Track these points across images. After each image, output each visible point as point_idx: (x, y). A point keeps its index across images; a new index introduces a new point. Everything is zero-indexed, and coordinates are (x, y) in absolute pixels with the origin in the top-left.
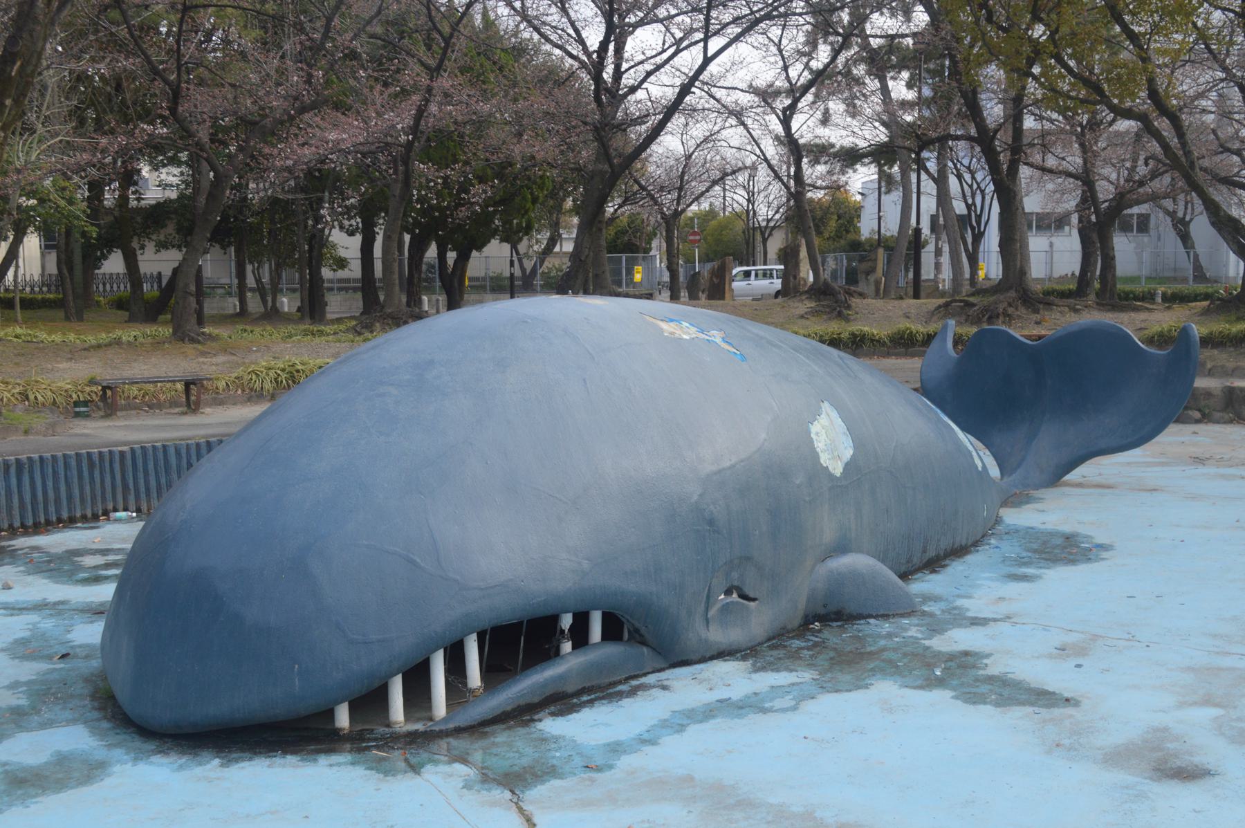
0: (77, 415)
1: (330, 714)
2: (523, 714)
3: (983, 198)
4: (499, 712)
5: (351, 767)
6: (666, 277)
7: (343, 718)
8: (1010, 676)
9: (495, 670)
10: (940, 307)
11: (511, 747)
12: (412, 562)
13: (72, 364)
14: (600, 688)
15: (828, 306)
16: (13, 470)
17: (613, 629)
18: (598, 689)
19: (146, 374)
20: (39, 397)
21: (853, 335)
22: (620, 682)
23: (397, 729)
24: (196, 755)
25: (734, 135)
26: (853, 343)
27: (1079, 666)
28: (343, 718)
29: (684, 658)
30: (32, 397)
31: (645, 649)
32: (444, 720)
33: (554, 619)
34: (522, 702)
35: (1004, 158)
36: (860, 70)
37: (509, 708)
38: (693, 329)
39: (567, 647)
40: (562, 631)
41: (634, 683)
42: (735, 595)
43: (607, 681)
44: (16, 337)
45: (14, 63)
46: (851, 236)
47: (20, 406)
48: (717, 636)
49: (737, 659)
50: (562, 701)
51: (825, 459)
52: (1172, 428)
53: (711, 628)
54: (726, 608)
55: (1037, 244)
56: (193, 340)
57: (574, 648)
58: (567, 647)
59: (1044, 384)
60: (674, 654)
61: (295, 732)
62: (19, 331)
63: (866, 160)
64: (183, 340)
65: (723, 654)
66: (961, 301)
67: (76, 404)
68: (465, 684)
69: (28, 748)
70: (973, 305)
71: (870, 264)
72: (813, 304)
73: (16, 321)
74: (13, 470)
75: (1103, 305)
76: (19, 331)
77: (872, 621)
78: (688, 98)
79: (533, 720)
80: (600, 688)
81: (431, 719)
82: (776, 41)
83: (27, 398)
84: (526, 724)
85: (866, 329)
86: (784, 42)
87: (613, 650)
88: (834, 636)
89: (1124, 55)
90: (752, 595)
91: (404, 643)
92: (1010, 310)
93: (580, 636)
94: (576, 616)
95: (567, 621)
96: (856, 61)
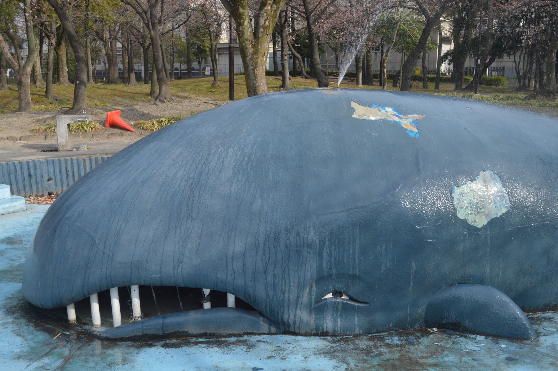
7: (72, 314)
28: (72, 314)
39: (207, 305)
43: (226, 332)
57: (212, 306)
58: (207, 305)
87: (237, 314)
93: (218, 298)
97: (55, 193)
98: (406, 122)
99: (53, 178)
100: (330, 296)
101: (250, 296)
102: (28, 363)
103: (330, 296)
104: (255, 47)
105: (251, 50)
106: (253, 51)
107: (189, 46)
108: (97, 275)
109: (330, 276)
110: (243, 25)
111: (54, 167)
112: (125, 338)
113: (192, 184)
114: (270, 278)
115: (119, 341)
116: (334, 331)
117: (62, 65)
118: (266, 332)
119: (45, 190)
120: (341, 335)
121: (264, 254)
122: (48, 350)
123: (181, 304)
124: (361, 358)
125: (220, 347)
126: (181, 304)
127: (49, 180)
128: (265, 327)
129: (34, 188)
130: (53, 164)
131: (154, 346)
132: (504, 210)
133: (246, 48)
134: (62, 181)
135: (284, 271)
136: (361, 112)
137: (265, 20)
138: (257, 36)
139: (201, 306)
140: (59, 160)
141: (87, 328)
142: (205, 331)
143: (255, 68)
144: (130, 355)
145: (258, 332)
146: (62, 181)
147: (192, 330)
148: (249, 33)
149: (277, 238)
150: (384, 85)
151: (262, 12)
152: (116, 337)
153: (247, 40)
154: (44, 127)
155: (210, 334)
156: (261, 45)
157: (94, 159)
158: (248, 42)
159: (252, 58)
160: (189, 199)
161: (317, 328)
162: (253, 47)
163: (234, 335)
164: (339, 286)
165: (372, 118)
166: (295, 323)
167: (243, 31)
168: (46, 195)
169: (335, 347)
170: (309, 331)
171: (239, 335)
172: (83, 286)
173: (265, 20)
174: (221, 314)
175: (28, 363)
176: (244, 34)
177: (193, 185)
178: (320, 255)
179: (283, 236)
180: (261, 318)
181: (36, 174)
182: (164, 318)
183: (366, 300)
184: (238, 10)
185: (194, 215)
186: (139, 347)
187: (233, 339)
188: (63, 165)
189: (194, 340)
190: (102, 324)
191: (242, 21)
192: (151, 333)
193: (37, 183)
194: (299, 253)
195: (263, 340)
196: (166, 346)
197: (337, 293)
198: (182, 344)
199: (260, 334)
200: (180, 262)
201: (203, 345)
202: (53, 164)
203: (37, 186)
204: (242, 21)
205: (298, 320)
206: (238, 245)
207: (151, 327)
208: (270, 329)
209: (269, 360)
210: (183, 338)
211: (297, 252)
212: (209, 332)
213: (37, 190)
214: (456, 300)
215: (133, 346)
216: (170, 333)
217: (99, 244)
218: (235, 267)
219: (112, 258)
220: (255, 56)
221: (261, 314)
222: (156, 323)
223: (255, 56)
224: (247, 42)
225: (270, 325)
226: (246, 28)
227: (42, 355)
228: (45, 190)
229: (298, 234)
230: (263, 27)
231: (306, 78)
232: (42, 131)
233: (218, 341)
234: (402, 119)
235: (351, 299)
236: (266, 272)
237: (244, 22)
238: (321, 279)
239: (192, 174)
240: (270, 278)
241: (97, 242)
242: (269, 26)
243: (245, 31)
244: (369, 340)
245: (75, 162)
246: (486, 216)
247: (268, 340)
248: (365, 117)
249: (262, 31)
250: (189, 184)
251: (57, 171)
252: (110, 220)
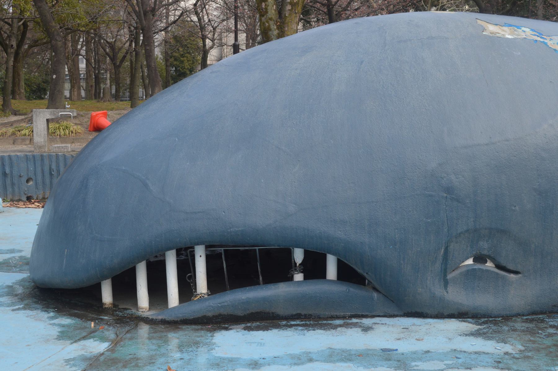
1: (96, 289)
6: (233, 28)
7: (107, 297)
8: (52, 314)
9: (216, 283)
12: (146, 185)
14: (307, 317)
17: (346, 273)
22: (338, 318)
23: (140, 313)
28: (107, 297)
29: (419, 310)
31: (375, 295)
33: (288, 253)
34: (229, 311)
37: (210, 314)
39: (299, 277)
42: (489, 265)
43: (327, 313)
48: (457, 296)
50: (262, 318)
53: (450, 289)
54: (470, 273)
57: (305, 278)
65: (461, 315)
87: (343, 289)
89: (36, 51)
90: (511, 267)
93: (314, 267)
94: (307, 253)
95: (298, 256)
97: (35, 198)
99: (34, 178)
102: (62, 347)
103: (470, 261)
106: (278, 34)
107: (168, 64)
111: (35, 164)
112: (190, 320)
115: (180, 324)
117: (19, 80)
118: (382, 314)
119: (22, 193)
120: (485, 317)
122: (84, 334)
123: (261, 278)
124: (527, 339)
125: (324, 329)
126: (261, 278)
127: (28, 181)
129: (10, 189)
130: (34, 160)
131: (231, 329)
133: (270, 30)
134: (44, 183)
138: (283, 16)
139: (291, 279)
141: (130, 313)
142: (299, 312)
144: (202, 339)
145: (370, 314)
146: (44, 183)
148: (273, 11)
152: (176, 319)
154: (11, 131)
155: (305, 315)
156: (288, 26)
158: (273, 22)
162: (278, 28)
164: (484, 246)
168: (25, 199)
169: (484, 328)
171: (344, 318)
174: (315, 288)
175: (62, 347)
181: (11, 172)
183: (519, 268)
186: (214, 330)
187: (338, 322)
188: (47, 162)
189: (284, 323)
190: (150, 309)
192: (225, 313)
193: (13, 184)
195: (380, 322)
196: (246, 329)
197: (480, 259)
198: (271, 327)
199: (373, 317)
201: (300, 328)
202: (34, 160)
203: (13, 188)
207: (226, 304)
209: (399, 342)
210: (268, 321)
212: (303, 313)
213: (13, 193)
215: (202, 329)
224: (271, 23)
226: (270, 5)
227: (78, 338)
228: (22, 193)
232: (9, 134)
233: (320, 324)
234: (546, 39)
235: (499, 267)
243: (269, 8)
244: (523, 322)
247: (388, 323)
249: (290, 8)
251: (39, 169)
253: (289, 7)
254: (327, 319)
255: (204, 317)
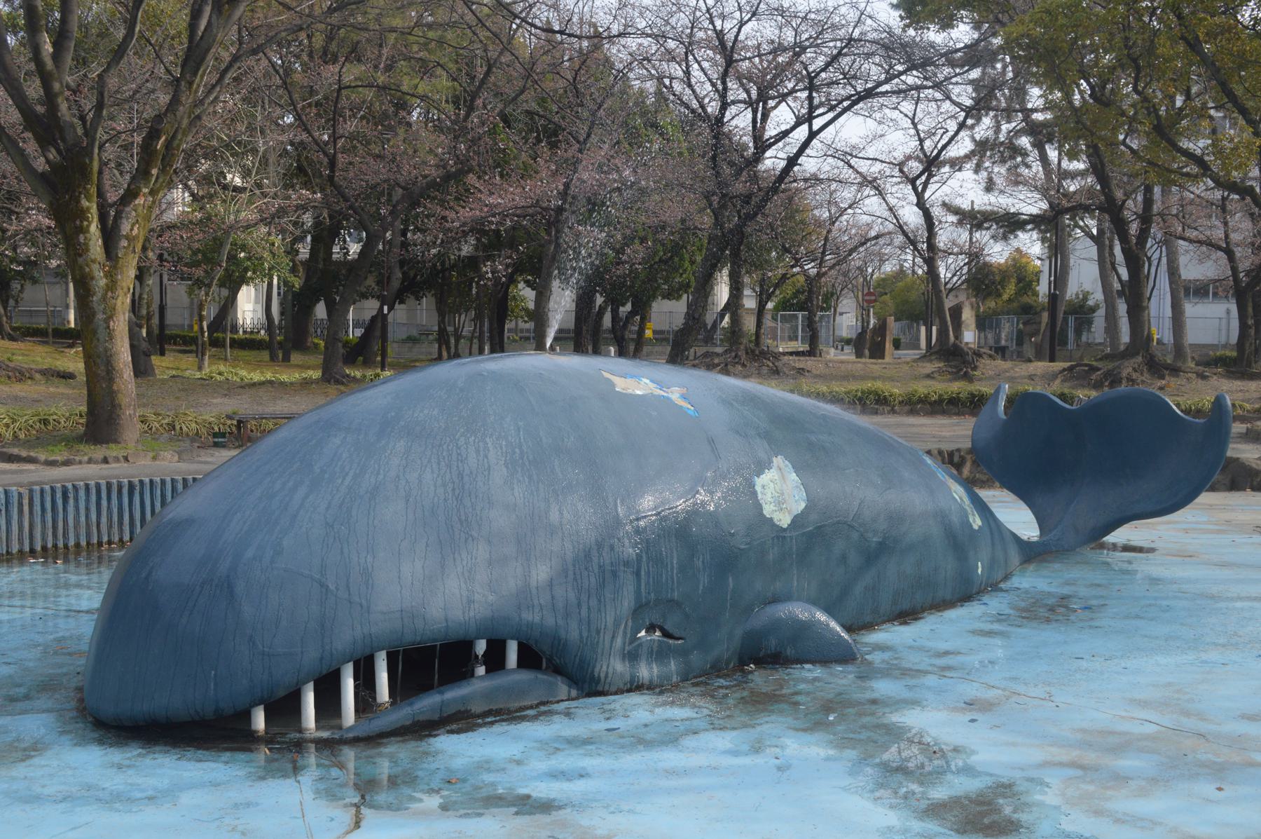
0: (216, 445)
1: (246, 716)
2: (423, 729)
3: (1150, 265)
4: (399, 725)
5: (94, 763)
7: (259, 721)
9: (403, 688)
10: (1064, 370)
11: (386, 760)
13: (226, 400)
15: (955, 367)
16: (125, 491)
17: (529, 658)
18: (504, 713)
19: (286, 411)
20: (185, 428)
21: (973, 396)
23: (307, 735)
24: (126, 744)
25: (873, 203)
26: (971, 402)
27: (973, 721)
28: (259, 721)
30: (178, 427)
32: (351, 728)
33: (468, 645)
35: (1134, 228)
36: (1025, 142)
38: (652, 385)
39: (481, 670)
40: (477, 657)
41: (543, 708)
43: (517, 705)
44: (220, 374)
45: (159, 138)
46: (1025, 299)
47: (166, 435)
49: (654, 694)
50: (461, 720)
51: (768, 510)
52: (1205, 498)
55: (1192, 309)
56: (338, 382)
57: (487, 671)
58: (481, 670)
59: (1093, 446)
60: (588, 684)
61: (209, 729)
62: (222, 368)
63: (1029, 227)
64: (329, 382)
66: (1086, 365)
67: (215, 435)
68: (374, 699)
69: (34, 724)
70: (1099, 369)
71: (1034, 326)
72: (941, 365)
73: (226, 360)
74: (125, 491)
75: (1233, 373)
76: (222, 368)
77: (807, 666)
78: (796, 169)
79: (430, 736)
80: (509, 712)
81: (340, 728)
82: (910, 115)
83: (174, 429)
84: (421, 738)
85: (984, 389)
86: (919, 115)
87: (526, 676)
88: (760, 679)
91: (311, 657)
92: (1134, 376)
93: (495, 660)
94: (489, 643)
95: (481, 647)
96: (1018, 133)
98: (675, 395)
100: (643, 633)
101: (560, 641)
103: (643, 633)
104: (110, 275)
105: (103, 282)
108: (346, 636)
109: (647, 603)
110: (88, 231)
113: (454, 490)
114: (584, 612)
116: (651, 681)
121: (575, 579)
128: (563, 689)
132: (803, 505)
133: (93, 278)
135: (599, 601)
136: (621, 384)
137: (133, 225)
140: (151, 481)
143: (110, 317)
147: (477, 708)
149: (588, 555)
150: (203, 354)
151: (127, 209)
153: (94, 261)
156: (122, 273)
157: (137, 483)
159: (104, 298)
160: (458, 510)
161: (632, 682)
162: (106, 276)
163: (531, 707)
164: (656, 618)
165: (639, 392)
166: (606, 676)
167: (86, 244)
170: (621, 686)
172: (322, 659)
173: (133, 225)
174: (499, 680)
176: (88, 250)
177: (457, 492)
178: (638, 574)
179: (594, 553)
180: (559, 678)
182: (442, 693)
184: (78, 202)
185: (474, 534)
187: (531, 712)
191: (85, 223)
194: (614, 574)
196: (452, 732)
200: (470, 601)
204: (85, 223)
205: (611, 670)
206: (541, 573)
208: (569, 692)
211: (609, 575)
214: (775, 626)
216: (449, 716)
217: (337, 589)
218: (542, 602)
219: (369, 607)
220: (110, 294)
221: (558, 670)
222: (427, 704)
223: (110, 294)
224: (95, 267)
225: (570, 687)
226: (94, 238)
229: (612, 548)
230: (127, 237)
231: (12, 339)
236: (579, 605)
237: (88, 226)
238: (639, 609)
239: (448, 476)
240: (584, 612)
241: (332, 587)
242: (137, 237)
243: (91, 243)
245: (104, 489)
246: (789, 512)
248: (630, 391)
250: (450, 490)
252: (342, 553)
253: (124, 243)
254: (516, 711)
255: (403, 727)
